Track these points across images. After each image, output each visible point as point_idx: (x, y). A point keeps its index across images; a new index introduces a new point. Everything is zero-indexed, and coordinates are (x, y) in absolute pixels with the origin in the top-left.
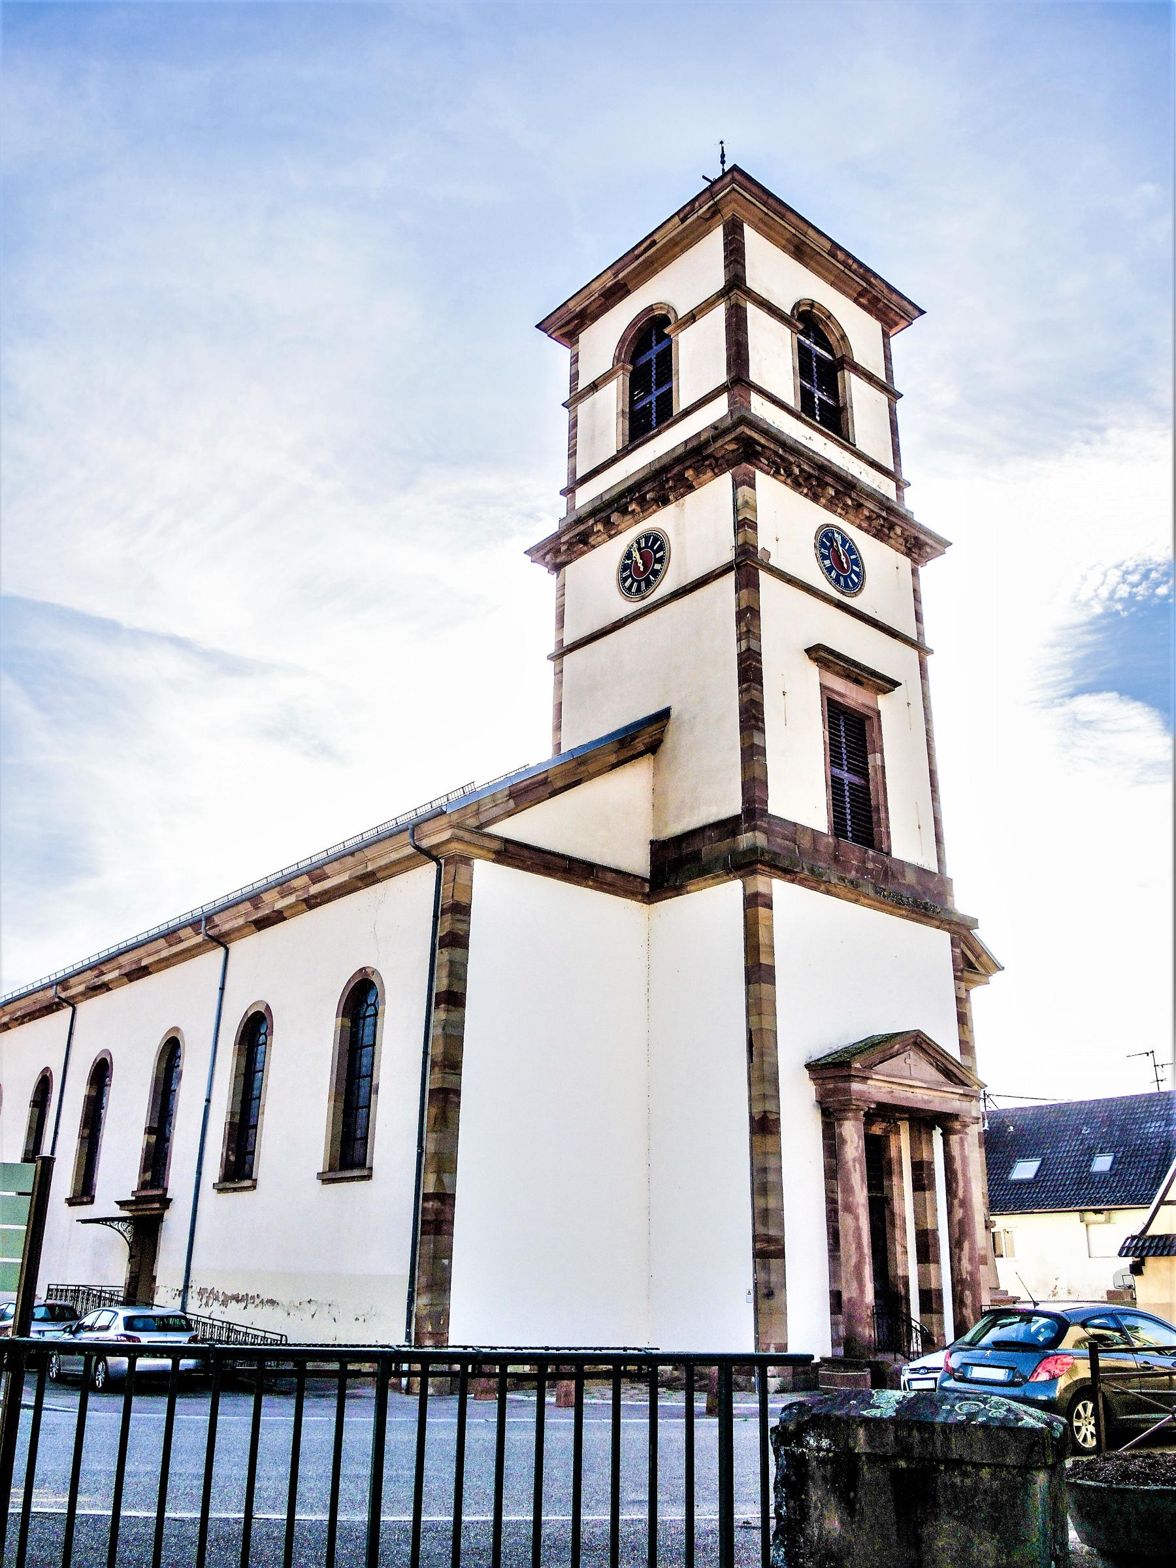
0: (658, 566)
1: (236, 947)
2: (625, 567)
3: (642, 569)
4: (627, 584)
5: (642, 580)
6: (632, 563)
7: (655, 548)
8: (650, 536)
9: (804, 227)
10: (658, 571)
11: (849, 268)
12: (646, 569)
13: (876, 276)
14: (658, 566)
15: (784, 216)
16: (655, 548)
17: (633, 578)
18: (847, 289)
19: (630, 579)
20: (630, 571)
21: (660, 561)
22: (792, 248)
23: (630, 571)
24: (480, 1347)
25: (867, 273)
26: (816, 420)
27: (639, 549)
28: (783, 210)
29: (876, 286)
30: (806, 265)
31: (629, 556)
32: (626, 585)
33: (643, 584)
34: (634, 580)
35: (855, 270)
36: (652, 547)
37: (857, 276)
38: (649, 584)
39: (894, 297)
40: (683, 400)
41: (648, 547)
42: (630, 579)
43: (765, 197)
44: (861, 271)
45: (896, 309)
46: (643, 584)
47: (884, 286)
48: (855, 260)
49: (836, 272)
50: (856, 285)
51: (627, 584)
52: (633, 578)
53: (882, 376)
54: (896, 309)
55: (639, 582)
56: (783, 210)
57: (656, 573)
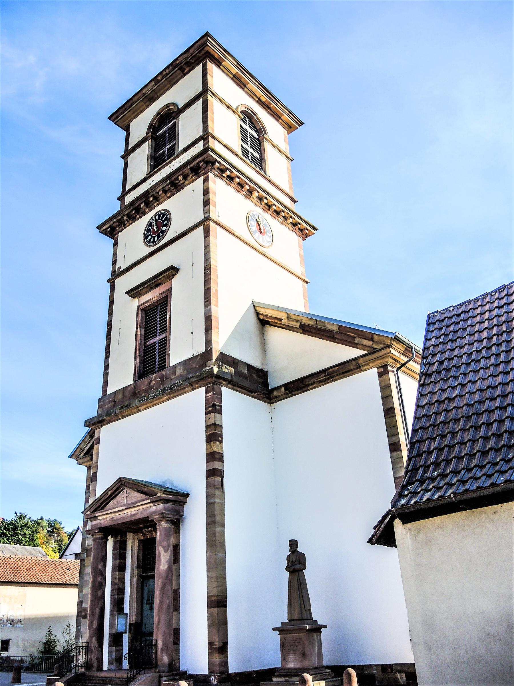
0: (164, 228)
1: (212, 215)
2: (149, 230)
3: (156, 230)
4: (148, 239)
5: (156, 236)
6: (151, 228)
7: (163, 220)
8: (161, 214)
9: (141, 94)
10: (165, 230)
11: (167, 74)
12: (158, 230)
13: (177, 59)
14: (164, 228)
15: (133, 102)
16: (163, 220)
17: (151, 236)
18: (141, 109)
19: (150, 236)
20: (163, 223)
21: (165, 225)
22: (148, 103)
23: (163, 223)
24: (395, 447)
25: (172, 65)
26: (200, 162)
27: (156, 220)
28: (131, 102)
29: (181, 61)
30: (158, 97)
31: (150, 224)
32: (148, 239)
33: (156, 238)
34: (152, 237)
35: (169, 71)
36: (161, 219)
37: (172, 71)
38: (159, 237)
39: (191, 51)
40: (181, 148)
41: (160, 220)
42: (150, 236)
43: (124, 109)
44: (171, 68)
45: (196, 52)
46: (156, 238)
47: (183, 56)
48: (165, 70)
49: (167, 82)
50: (128, 114)
51: (148, 239)
52: (151, 236)
53: (128, 188)
54: (196, 52)
55: (154, 237)
56: (131, 102)
57: (163, 232)
